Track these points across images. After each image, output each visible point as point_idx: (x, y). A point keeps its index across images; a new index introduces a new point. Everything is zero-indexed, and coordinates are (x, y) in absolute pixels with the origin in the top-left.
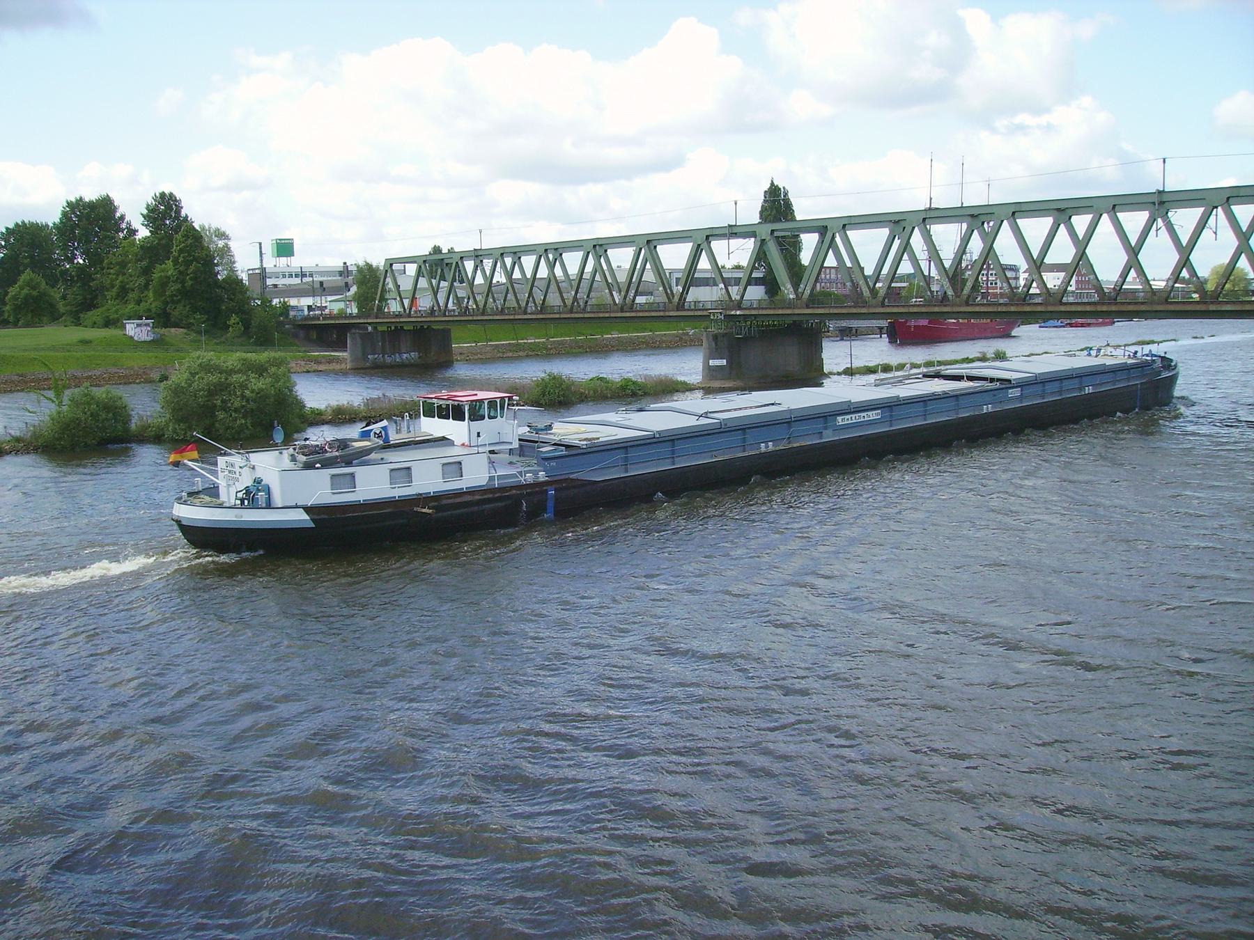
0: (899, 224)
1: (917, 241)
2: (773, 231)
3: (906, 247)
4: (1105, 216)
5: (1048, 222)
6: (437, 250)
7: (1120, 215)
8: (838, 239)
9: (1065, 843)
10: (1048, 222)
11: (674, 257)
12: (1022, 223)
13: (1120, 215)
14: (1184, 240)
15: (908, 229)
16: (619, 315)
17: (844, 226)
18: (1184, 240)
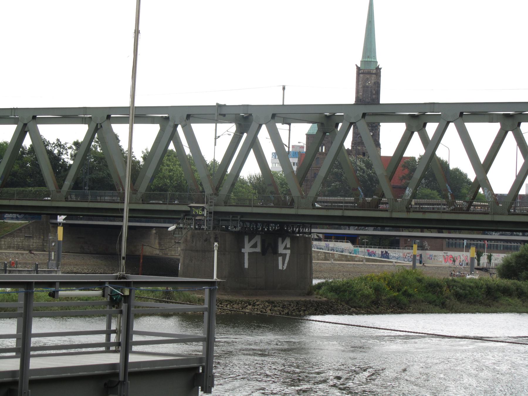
0: (246, 119)
1: (264, 136)
2: (364, 115)
3: (254, 144)
4: (452, 126)
5: (496, 127)
6: (217, 104)
7: (469, 126)
8: (180, 129)
9: (407, 337)
10: (496, 127)
11: (139, 140)
12: (471, 127)
13: (469, 126)
14: (482, 157)
15: (254, 126)
16: (404, 215)
17: (188, 116)
18: (482, 157)
